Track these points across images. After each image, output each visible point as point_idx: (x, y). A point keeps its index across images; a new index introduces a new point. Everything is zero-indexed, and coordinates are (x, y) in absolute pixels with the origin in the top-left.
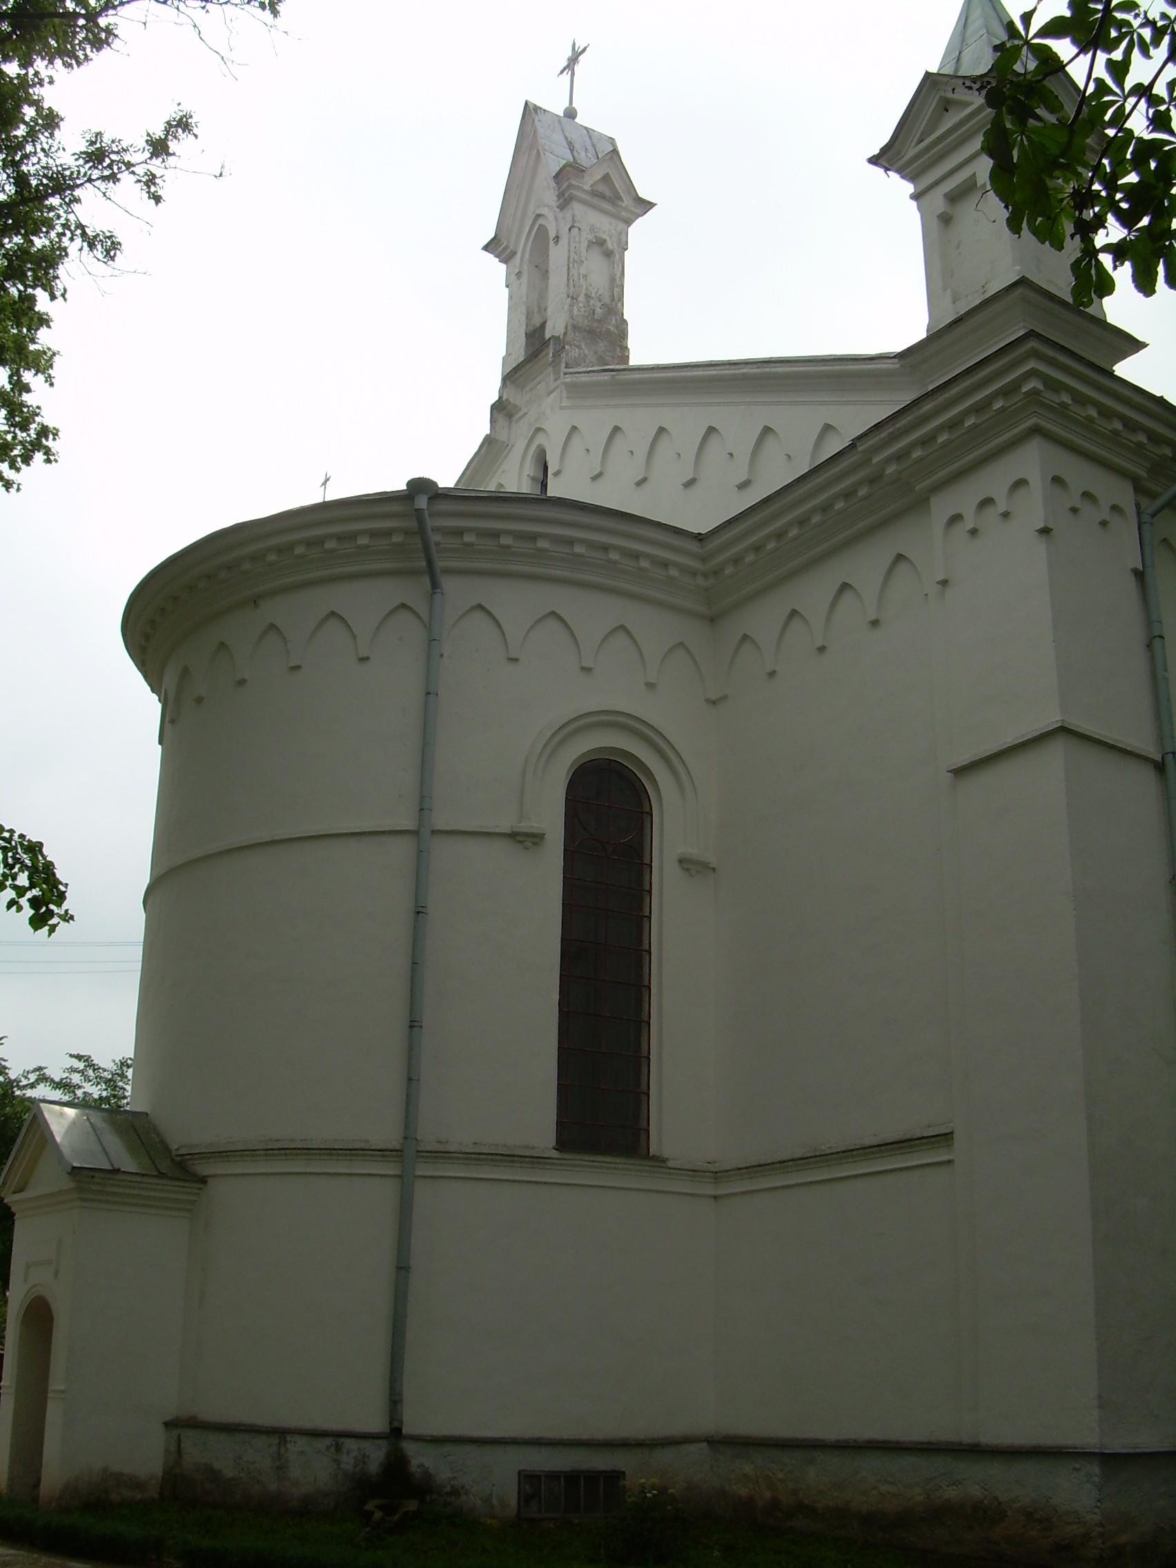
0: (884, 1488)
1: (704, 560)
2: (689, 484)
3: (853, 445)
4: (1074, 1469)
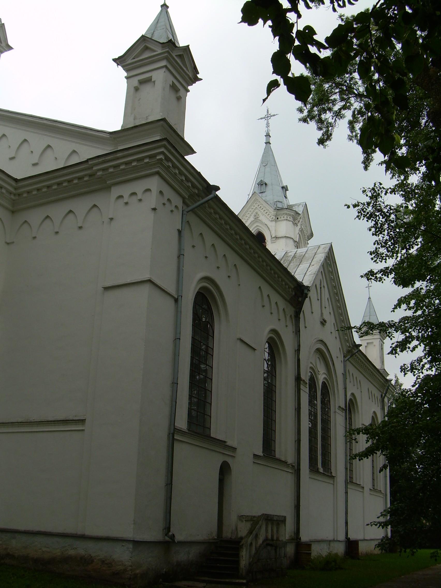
0: (44, 549)
1: (16, 189)
2: (12, 159)
3: (87, 161)
4: (123, 546)
